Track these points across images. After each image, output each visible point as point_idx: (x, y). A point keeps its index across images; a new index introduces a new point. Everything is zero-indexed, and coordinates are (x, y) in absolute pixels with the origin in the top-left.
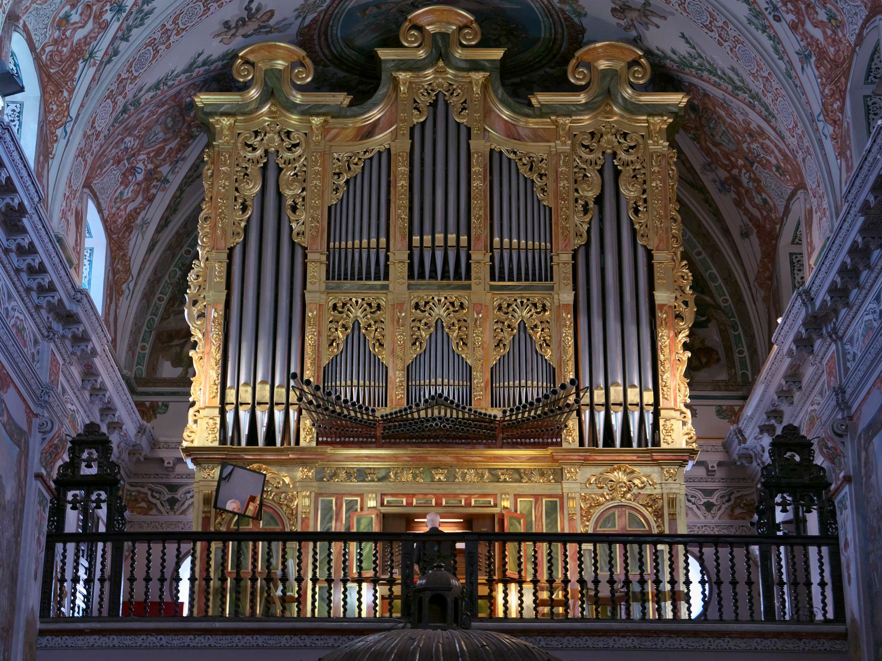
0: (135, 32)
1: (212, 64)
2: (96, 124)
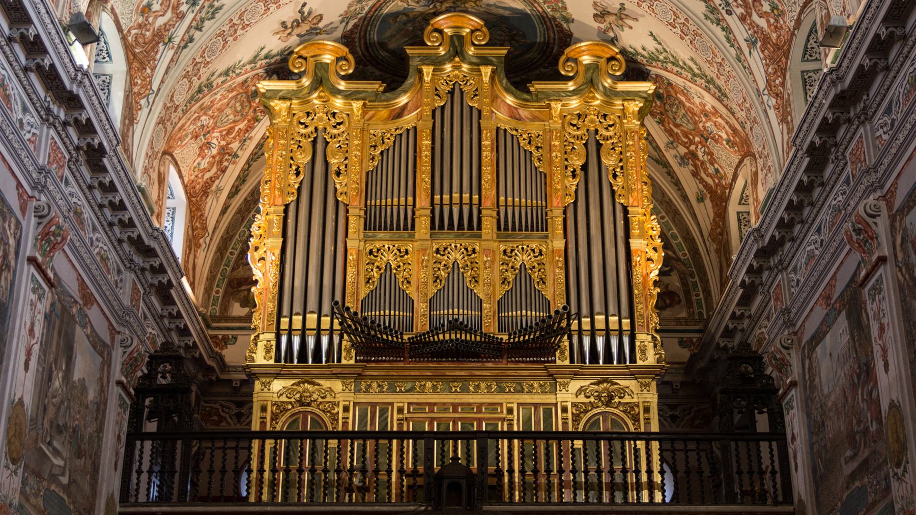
0: (207, 24)
2: (174, 99)
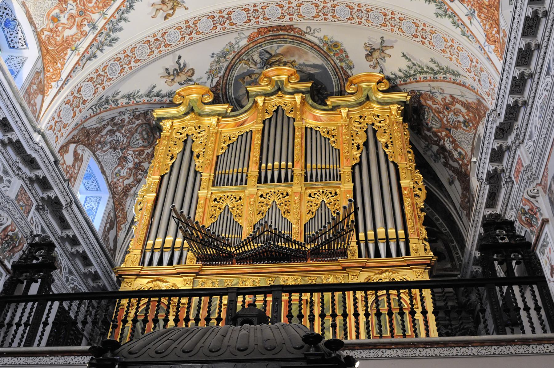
1: (163, 97)
